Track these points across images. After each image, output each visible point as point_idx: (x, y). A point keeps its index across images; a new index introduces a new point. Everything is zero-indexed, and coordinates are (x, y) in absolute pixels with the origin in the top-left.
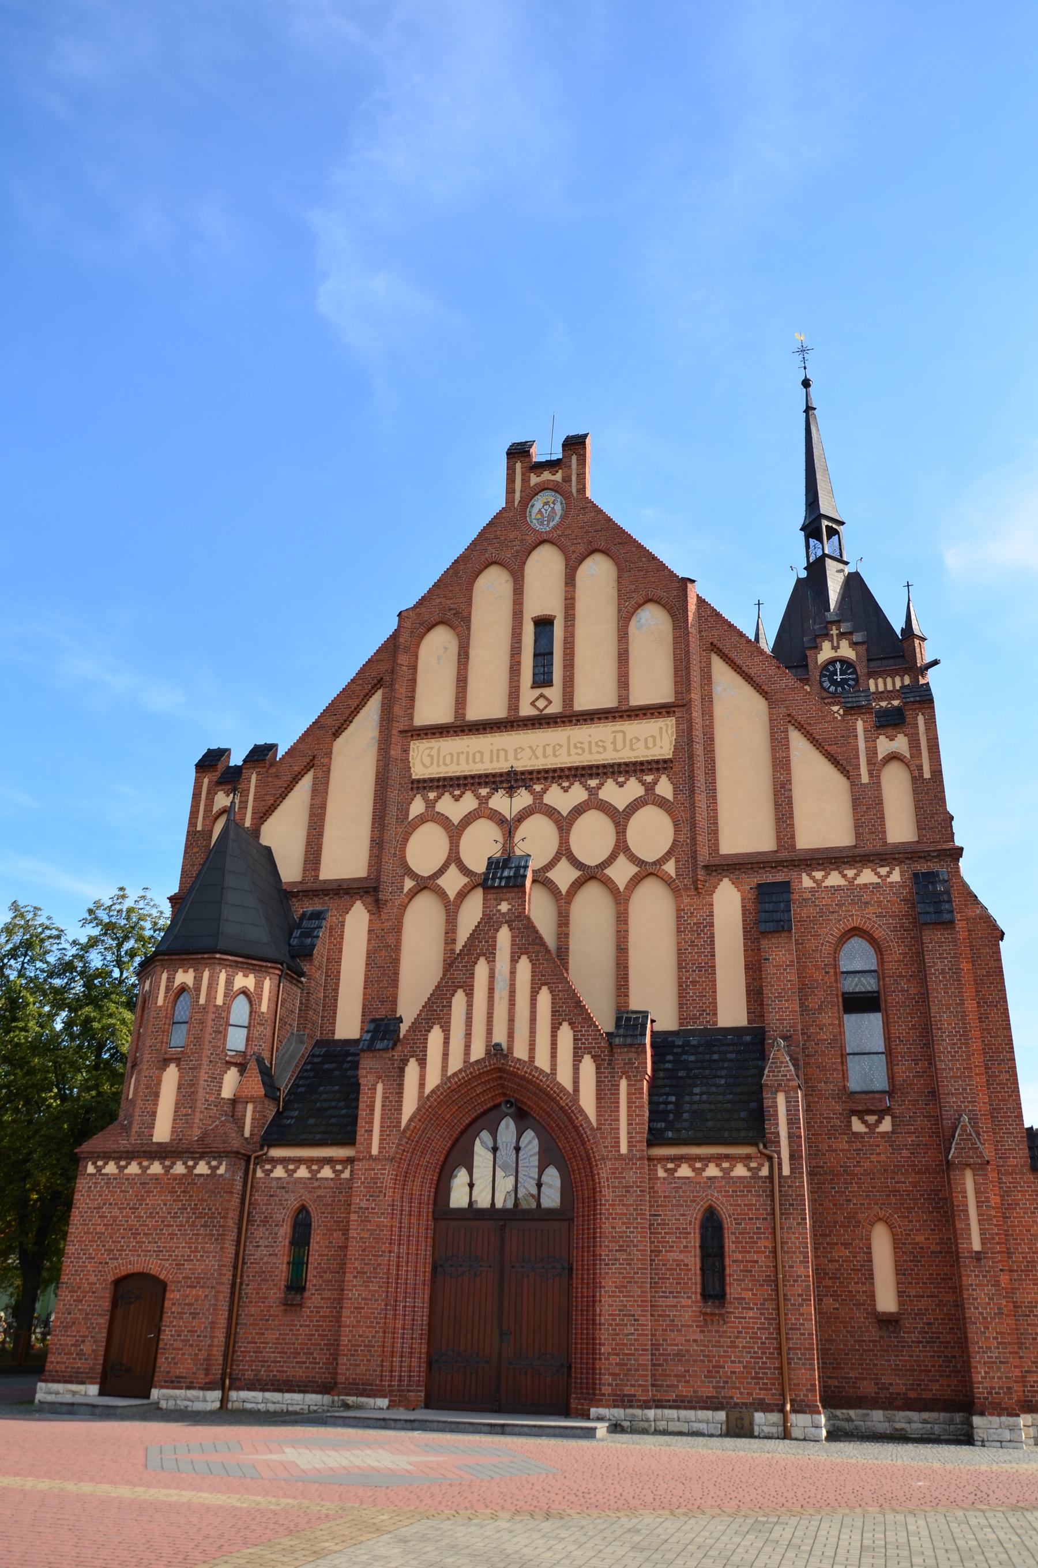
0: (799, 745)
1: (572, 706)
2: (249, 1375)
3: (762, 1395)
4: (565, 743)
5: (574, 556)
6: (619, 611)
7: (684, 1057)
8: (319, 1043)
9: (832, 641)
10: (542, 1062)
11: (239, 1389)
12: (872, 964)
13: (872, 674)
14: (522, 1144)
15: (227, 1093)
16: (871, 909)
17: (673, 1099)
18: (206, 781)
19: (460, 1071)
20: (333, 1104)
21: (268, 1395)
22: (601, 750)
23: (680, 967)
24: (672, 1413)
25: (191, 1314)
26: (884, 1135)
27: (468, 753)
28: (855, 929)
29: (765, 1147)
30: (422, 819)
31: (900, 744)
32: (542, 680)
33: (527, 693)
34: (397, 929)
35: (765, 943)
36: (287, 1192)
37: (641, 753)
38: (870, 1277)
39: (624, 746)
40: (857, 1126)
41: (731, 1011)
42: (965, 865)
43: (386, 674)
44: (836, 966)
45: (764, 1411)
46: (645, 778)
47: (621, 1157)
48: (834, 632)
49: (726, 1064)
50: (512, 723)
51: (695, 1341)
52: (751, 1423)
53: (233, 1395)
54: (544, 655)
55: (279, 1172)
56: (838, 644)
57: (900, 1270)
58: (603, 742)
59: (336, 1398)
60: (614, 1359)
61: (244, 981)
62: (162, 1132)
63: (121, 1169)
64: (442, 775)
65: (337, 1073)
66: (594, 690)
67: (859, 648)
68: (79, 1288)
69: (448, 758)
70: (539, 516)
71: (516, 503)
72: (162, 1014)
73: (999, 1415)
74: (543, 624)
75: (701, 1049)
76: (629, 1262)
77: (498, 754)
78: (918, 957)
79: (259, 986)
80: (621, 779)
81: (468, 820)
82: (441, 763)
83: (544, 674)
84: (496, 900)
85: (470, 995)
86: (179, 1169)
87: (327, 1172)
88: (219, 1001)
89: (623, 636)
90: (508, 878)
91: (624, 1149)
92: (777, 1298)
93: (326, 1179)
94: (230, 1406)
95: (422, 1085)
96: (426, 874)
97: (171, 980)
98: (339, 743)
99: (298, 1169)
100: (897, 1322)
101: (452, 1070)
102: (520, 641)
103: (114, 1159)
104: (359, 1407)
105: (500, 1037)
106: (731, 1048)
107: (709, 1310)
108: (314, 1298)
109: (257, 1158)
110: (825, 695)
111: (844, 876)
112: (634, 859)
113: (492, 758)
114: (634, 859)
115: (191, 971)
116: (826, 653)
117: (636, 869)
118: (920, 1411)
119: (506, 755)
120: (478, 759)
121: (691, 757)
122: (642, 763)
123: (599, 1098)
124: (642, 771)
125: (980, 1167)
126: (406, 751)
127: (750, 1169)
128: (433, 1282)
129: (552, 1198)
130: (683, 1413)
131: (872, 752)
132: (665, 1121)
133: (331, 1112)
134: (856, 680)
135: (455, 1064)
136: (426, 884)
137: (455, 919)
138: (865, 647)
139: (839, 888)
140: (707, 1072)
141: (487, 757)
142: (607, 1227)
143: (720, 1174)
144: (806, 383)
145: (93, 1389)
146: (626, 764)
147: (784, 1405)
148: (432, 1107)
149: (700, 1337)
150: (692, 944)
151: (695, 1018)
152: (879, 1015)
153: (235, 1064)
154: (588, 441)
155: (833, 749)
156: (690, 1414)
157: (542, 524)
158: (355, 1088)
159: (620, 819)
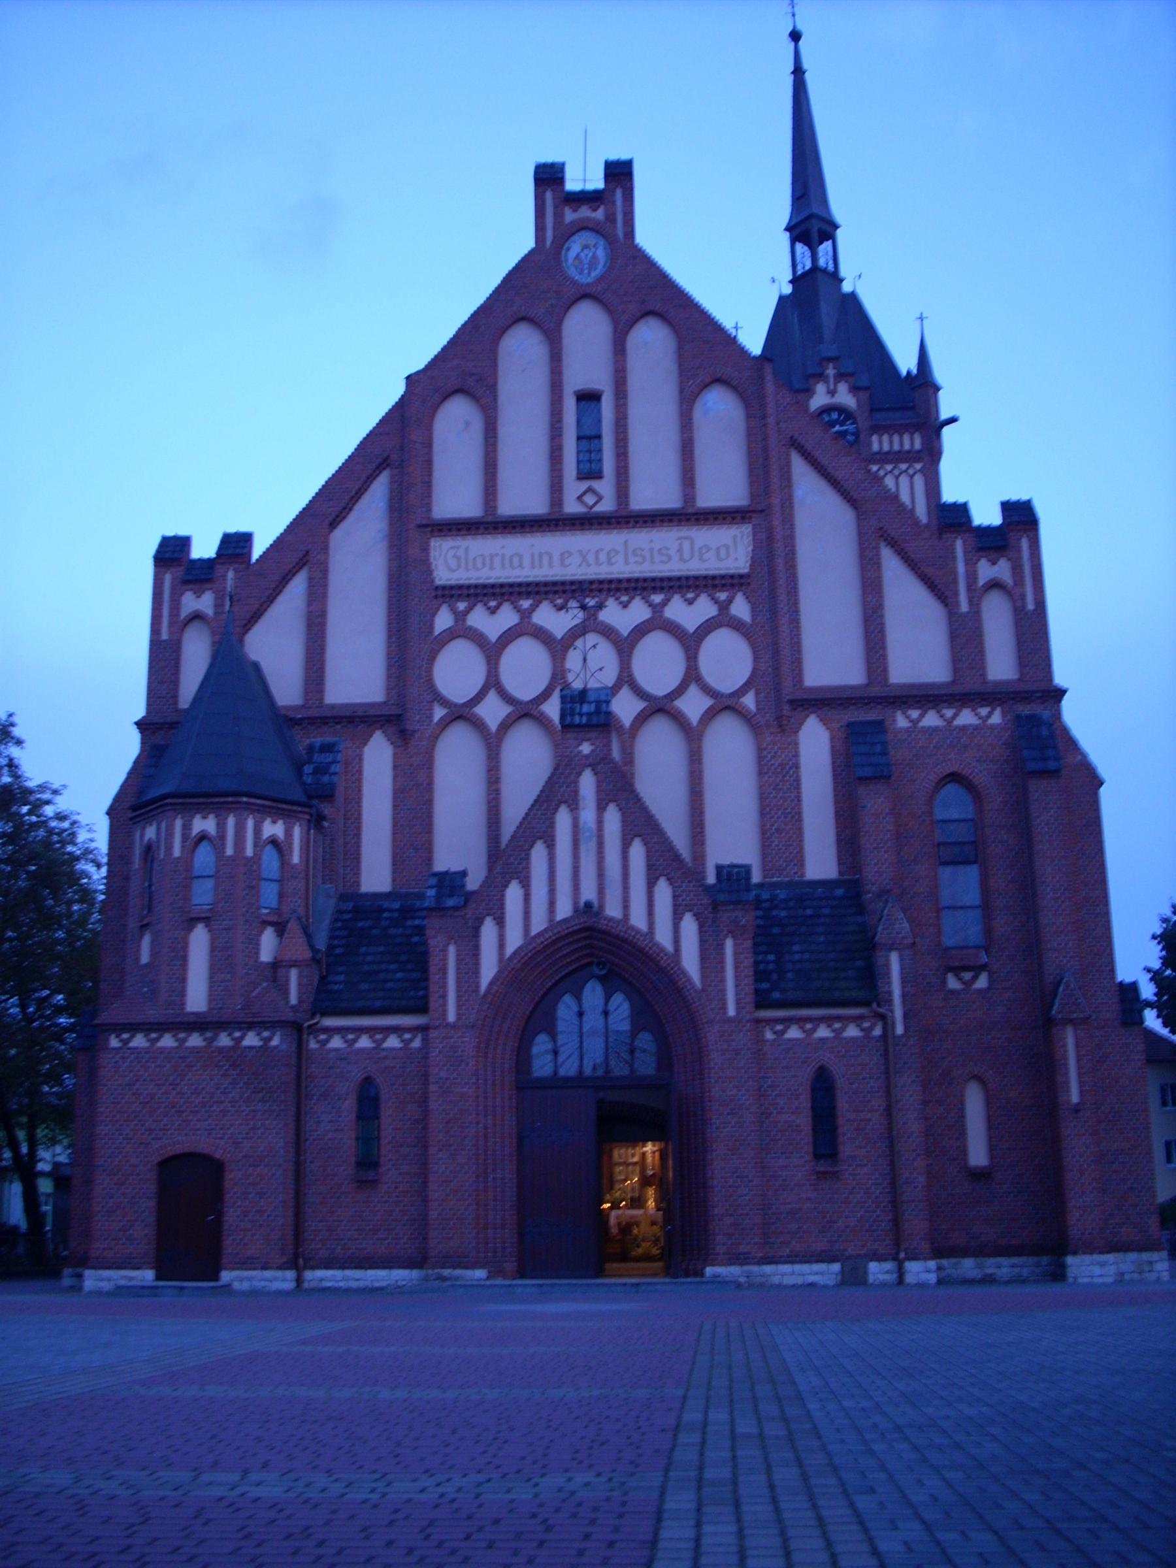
1: (627, 504)
6: (681, 391)
7: (774, 913)
8: (343, 897)
10: (638, 920)
11: (313, 1268)
12: (968, 811)
13: (877, 429)
15: (266, 956)
17: (771, 957)
18: (168, 578)
19: (546, 930)
20: (384, 966)
22: (665, 558)
24: (786, 1268)
25: (257, 1193)
26: (980, 991)
27: (503, 556)
29: (879, 1005)
30: (451, 635)
31: (1001, 570)
33: (573, 488)
34: (428, 765)
35: (862, 790)
36: (349, 1063)
37: (711, 565)
38: (962, 1133)
40: (953, 983)
41: (820, 861)
42: (1066, 704)
43: (394, 451)
44: (931, 814)
46: (718, 594)
47: (730, 1020)
48: (831, 371)
49: (822, 920)
50: (553, 522)
51: (808, 1199)
53: (309, 1275)
54: (590, 438)
55: (336, 1042)
57: (991, 1124)
58: (668, 549)
59: (430, 1272)
61: (273, 829)
62: (197, 998)
64: (481, 581)
65: (375, 932)
66: (654, 489)
73: (1091, 1253)
74: (588, 398)
75: (791, 904)
78: (1020, 807)
79: (288, 833)
80: (690, 595)
82: (470, 564)
83: (590, 461)
84: (576, 739)
85: (551, 845)
86: (224, 1040)
87: (393, 1042)
88: (249, 852)
90: (589, 714)
91: (731, 1011)
94: (306, 1285)
95: (501, 945)
97: (187, 827)
99: (356, 1040)
102: (560, 420)
103: (142, 1031)
104: (457, 1278)
105: (588, 893)
107: (822, 1169)
109: (310, 1026)
112: (707, 689)
114: (707, 689)
116: (820, 398)
121: (772, 572)
122: (714, 577)
126: (426, 550)
131: (972, 577)
133: (382, 976)
134: (857, 434)
135: (539, 923)
136: (462, 714)
139: (936, 729)
140: (803, 929)
141: (527, 562)
144: (795, 36)
146: (696, 578)
147: (897, 1253)
148: (515, 971)
156: (805, 1268)
157: (581, 273)
159: (691, 642)
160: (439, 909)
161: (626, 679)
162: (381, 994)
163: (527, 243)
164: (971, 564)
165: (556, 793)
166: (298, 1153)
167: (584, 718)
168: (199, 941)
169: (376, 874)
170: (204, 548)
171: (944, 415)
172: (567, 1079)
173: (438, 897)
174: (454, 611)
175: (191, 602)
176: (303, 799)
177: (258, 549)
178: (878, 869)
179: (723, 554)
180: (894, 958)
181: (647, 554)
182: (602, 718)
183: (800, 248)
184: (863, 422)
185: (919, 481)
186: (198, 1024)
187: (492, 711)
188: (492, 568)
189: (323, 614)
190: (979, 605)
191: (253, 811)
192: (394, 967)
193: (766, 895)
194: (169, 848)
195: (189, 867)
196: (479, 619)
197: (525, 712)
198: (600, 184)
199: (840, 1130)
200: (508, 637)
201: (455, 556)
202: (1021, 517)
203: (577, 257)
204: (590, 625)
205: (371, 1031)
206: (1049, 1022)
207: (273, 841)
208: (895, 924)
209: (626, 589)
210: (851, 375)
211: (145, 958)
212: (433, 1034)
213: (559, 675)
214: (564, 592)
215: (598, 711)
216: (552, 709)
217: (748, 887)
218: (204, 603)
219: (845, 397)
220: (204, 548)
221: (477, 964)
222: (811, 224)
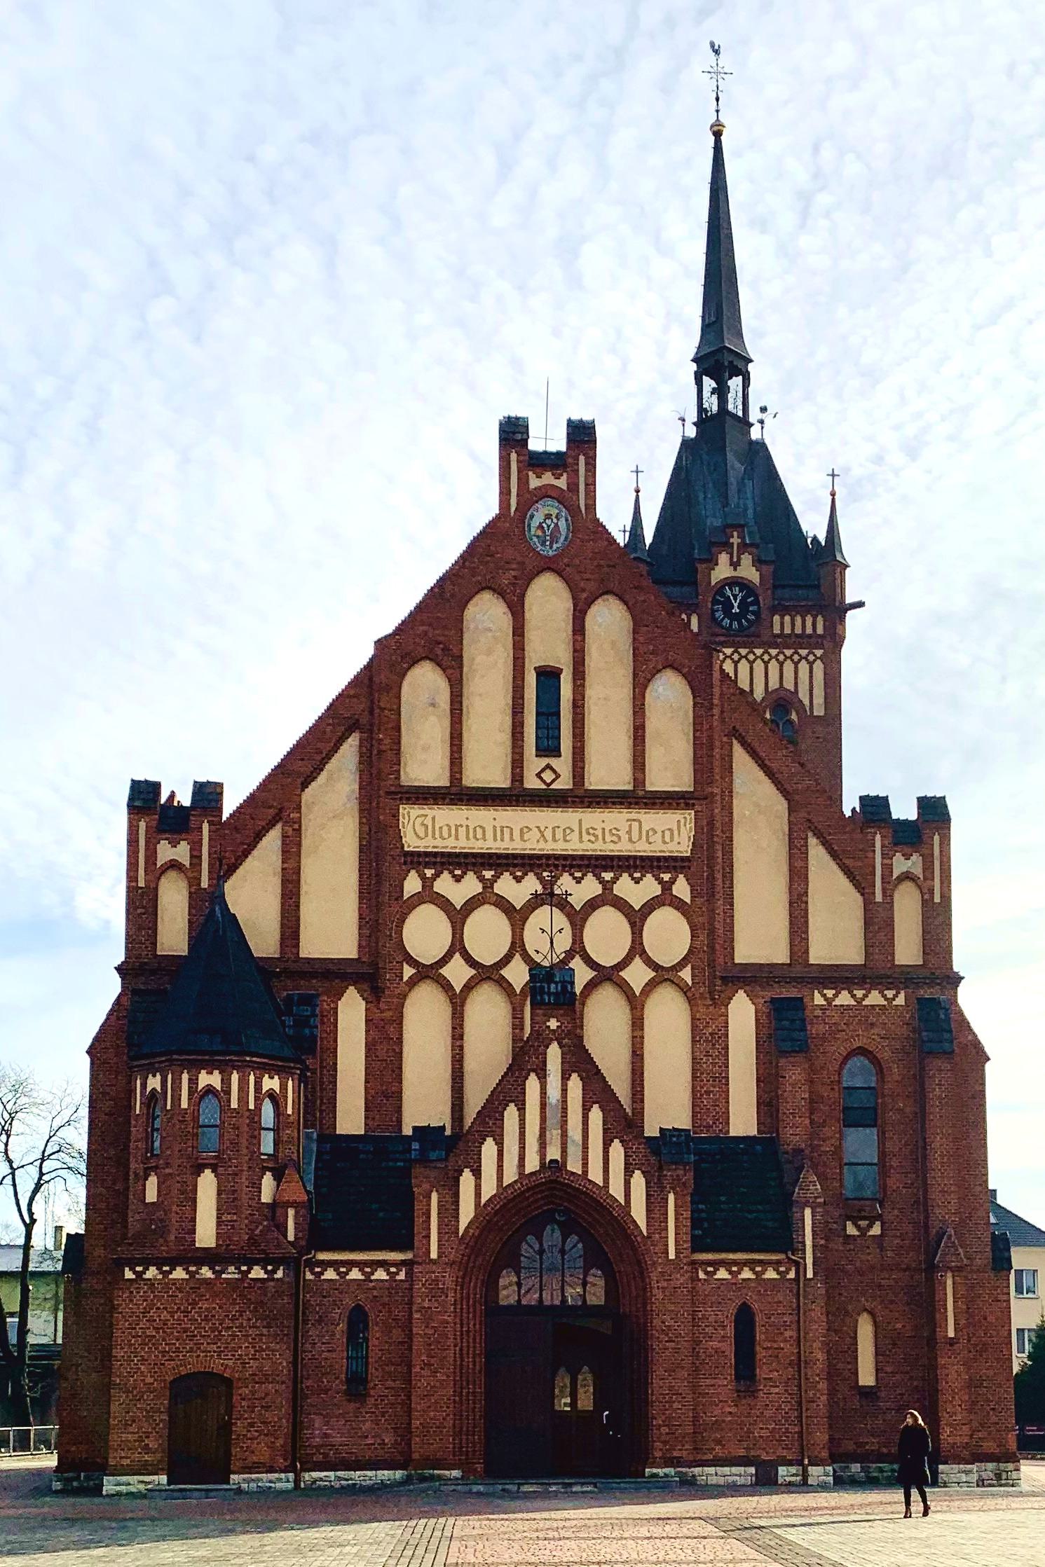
5: (584, 595)
6: (635, 675)
10: (595, 1175)
13: (781, 609)
14: (567, 1248)
16: (875, 1031)
18: (142, 825)
21: (339, 1473)
23: (694, 1078)
30: (418, 900)
31: (913, 864)
32: (548, 747)
33: (534, 764)
34: (399, 1020)
39: (640, 838)
40: (851, 1230)
41: (743, 1120)
42: (962, 991)
43: (364, 713)
44: (839, 1082)
50: (514, 796)
55: (330, 1274)
60: (665, 1430)
61: (271, 1084)
62: (206, 1234)
63: (166, 1274)
66: (609, 770)
67: (764, 567)
71: (513, 509)
74: (549, 676)
76: (677, 1351)
77: (502, 831)
79: (283, 1087)
80: (637, 875)
82: (437, 835)
85: (522, 1109)
86: (231, 1273)
87: (381, 1274)
90: (556, 994)
96: (428, 961)
97: (193, 1082)
98: (308, 795)
99: (349, 1269)
105: (553, 1153)
108: (379, 1386)
110: (718, 630)
112: (650, 962)
114: (650, 962)
115: (216, 1072)
116: (723, 570)
121: (712, 858)
123: (649, 1211)
124: (659, 867)
125: (956, 1271)
126: (396, 816)
129: (596, 1296)
135: (510, 1176)
136: (429, 973)
137: (462, 1014)
138: (772, 568)
141: (489, 834)
143: (753, 1277)
145: (164, 1479)
147: (802, 1460)
148: (490, 1215)
149: (733, 1410)
151: (709, 1127)
152: (875, 1130)
153: (270, 1169)
156: (726, 1470)
157: (543, 544)
158: (409, 1199)
159: (637, 918)
160: (424, 1160)
161: (578, 948)
165: (525, 1058)
168: (207, 1184)
169: (350, 1118)
171: (849, 600)
172: (529, 1307)
175: (166, 852)
177: (230, 804)
178: (794, 1134)
180: (808, 1212)
185: (819, 667)
188: (457, 839)
189: (298, 871)
190: (892, 896)
191: (253, 1069)
194: (177, 1099)
195: (196, 1118)
197: (488, 974)
198: (562, 447)
200: (472, 904)
202: (934, 812)
203: (540, 527)
206: (931, 1268)
211: (151, 1195)
218: (182, 852)
219: (749, 571)
222: (720, 358)
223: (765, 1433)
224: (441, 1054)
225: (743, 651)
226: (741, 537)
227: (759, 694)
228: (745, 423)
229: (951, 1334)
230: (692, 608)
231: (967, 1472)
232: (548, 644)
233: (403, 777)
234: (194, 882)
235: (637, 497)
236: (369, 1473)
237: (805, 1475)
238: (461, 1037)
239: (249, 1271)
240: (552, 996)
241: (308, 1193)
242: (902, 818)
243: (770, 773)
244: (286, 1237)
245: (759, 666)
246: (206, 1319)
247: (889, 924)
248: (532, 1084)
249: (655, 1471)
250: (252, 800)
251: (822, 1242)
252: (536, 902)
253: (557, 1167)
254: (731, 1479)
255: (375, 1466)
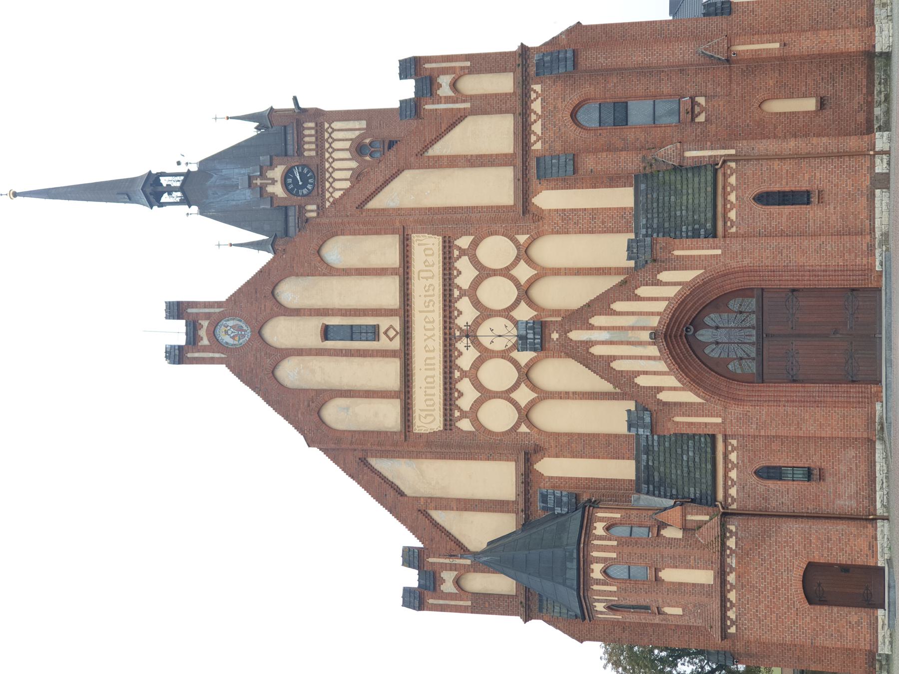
0: (439, 149)
2: (866, 503)
3: (865, 168)
4: (425, 314)
6: (324, 275)
7: (655, 226)
9: (267, 184)
10: (661, 306)
13: (300, 151)
14: (714, 325)
15: (679, 534)
16: (559, 105)
18: (431, 601)
19: (666, 362)
21: (878, 488)
23: (592, 232)
28: (571, 116)
30: (475, 421)
31: (445, 81)
32: (373, 333)
33: (383, 343)
34: (557, 435)
40: (701, 118)
41: (623, 198)
43: (355, 455)
45: (874, 167)
51: (835, 208)
52: (882, 174)
55: (733, 492)
56: (270, 179)
57: (790, 96)
60: (847, 256)
61: (599, 529)
62: (705, 577)
63: (732, 605)
66: (386, 293)
67: (274, 162)
68: (814, 629)
69: (428, 403)
70: (237, 338)
71: (223, 356)
72: (623, 586)
74: (326, 333)
75: (649, 216)
77: (428, 365)
79: (602, 520)
80: (455, 273)
81: (478, 385)
85: (614, 358)
86: (732, 561)
87: (733, 457)
88: (615, 543)
89: (346, 272)
90: (534, 334)
91: (718, 252)
92: (808, 156)
93: (738, 456)
95: (675, 389)
97: (598, 582)
99: (734, 482)
100: (821, 98)
101: (665, 368)
103: (726, 612)
104: (881, 418)
105: (645, 336)
106: (649, 196)
108: (815, 460)
109: (723, 508)
110: (315, 193)
111: (535, 121)
112: (515, 263)
113: (431, 369)
114: (515, 263)
116: (277, 190)
117: (522, 262)
118: (874, 86)
119: (430, 358)
120: (432, 380)
122: (444, 258)
126: (421, 435)
127: (732, 174)
128: (802, 382)
130: (877, 215)
131: (448, 100)
132: (699, 230)
134: (304, 166)
135: (661, 366)
136: (525, 414)
139: (543, 125)
141: (430, 373)
142: (768, 262)
143: (734, 193)
145: (880, 612)
148: (693, 380)
150: (576, 223)
151: (627, 222)
153: (659, 531)
154: (525, 43)
155: (444, 127)
156: (877, 211)
157: (244, 336)
159: (484, 273)
161: (506, 313)
162: (703, 466)
163: (222, 370)
164: (439, 100)
165: (581, 354)
166: (802, 517)
167: (538, 336)
168: (670, 575)
169: (623, 470)
170: (411, 578)
171: (292, 106)
173: (644, 427)
174: (460, 418)
175: (448, 587)
176: (578, 514)
177: (417, 543)
178: (631, 162)
179: (430, 252)
180: (688, 154)
181: (428, 299)
182: (538, 326)
183: (165, 198)
184: (295, 162)
185: (336, 125)
186: (722, 575)
187: (524, 395)
189: (459, 500)
192: (685, 458)
193: (644, 231)
194: (611, 593)
196: (465, 403)
197: (525, 375)
199: (793, 189)
200: (478, 385)
201: (425, 418)
202: (411, 67)
203: (233, 338)
204: (471, 334)
205: (726, 471)
207: (608, 529)
208: (668, 153)
209: (450, 312)
210: (261, 168)
211: (678, 611)
212: (729, 432)
213: (504, 354)
214: (450, 350)
215: (533, 328)
216: (524, 357)
217: (636, 241)
218: (448, 576)
220: (411, 578)
221: (686, 404)
222: (151, 190)
223: (850, 182)
224: (578, 409)
225: (327, 175)
226: (256, 178)
227: (354, 164)
228: (188, 175)
229: (777, 45)
230: (302, 209)
231: (882, 31)
232: (306, 333)
233: (395, 430)
234: (467, 569)
235: (235, 245)
236: (878, 468)
237: (882, 152)
238: (567, 393)
239: (731, 549)
240: (538, 336)
241: (674, 505)
242: (414, 90)
243: (386, 183)
244: (706, 522)
245: (336, 165)
246: (764, 578)
247: (485, 97)
248: (597, 350)
249: (877, 263)
250: (413, 529)
251: (709, 143)
252: (477, 344)
253: (654, 335)
254: (884, 207)
255: (872, 464)
